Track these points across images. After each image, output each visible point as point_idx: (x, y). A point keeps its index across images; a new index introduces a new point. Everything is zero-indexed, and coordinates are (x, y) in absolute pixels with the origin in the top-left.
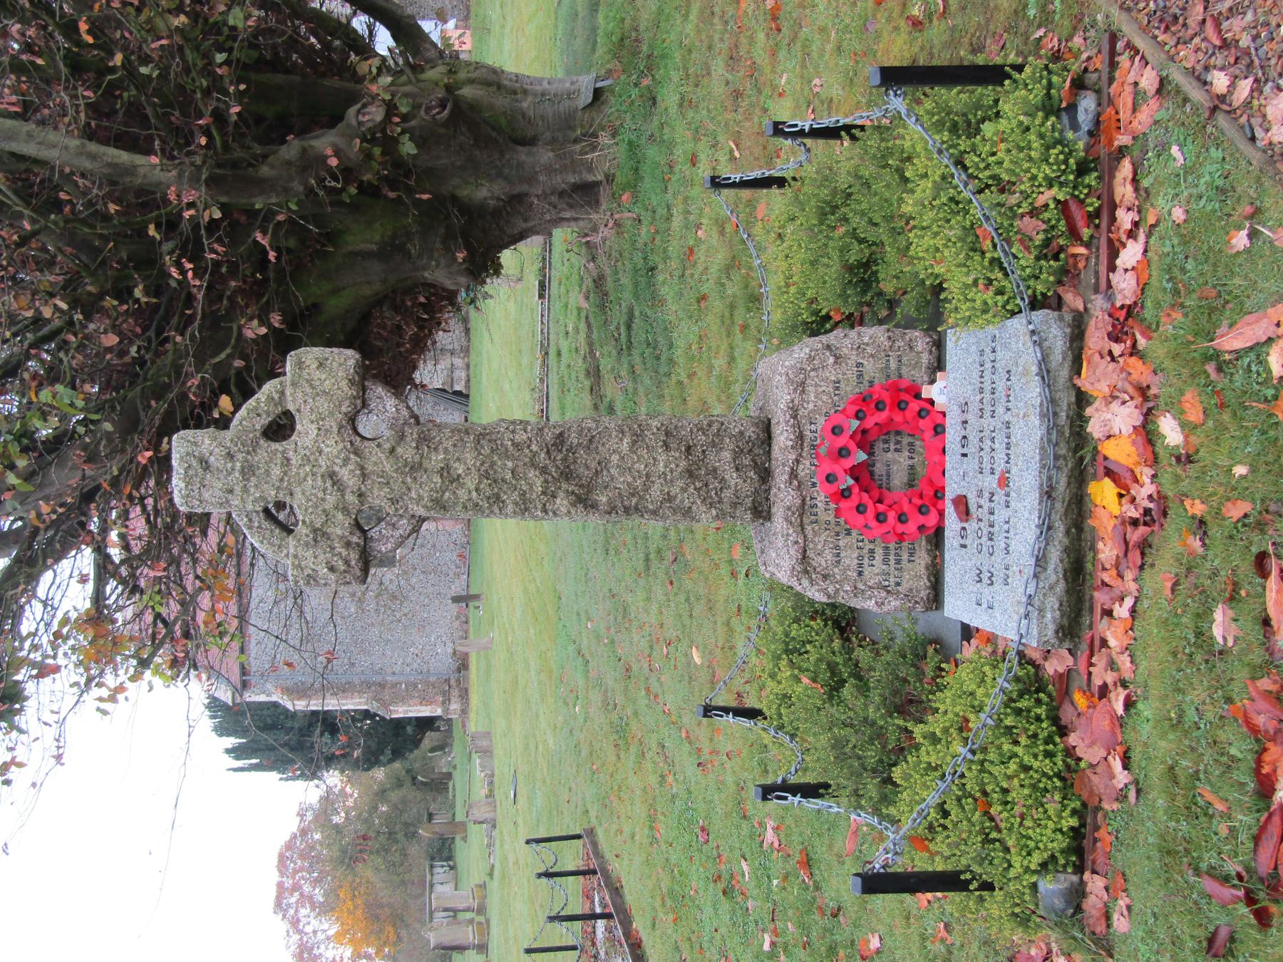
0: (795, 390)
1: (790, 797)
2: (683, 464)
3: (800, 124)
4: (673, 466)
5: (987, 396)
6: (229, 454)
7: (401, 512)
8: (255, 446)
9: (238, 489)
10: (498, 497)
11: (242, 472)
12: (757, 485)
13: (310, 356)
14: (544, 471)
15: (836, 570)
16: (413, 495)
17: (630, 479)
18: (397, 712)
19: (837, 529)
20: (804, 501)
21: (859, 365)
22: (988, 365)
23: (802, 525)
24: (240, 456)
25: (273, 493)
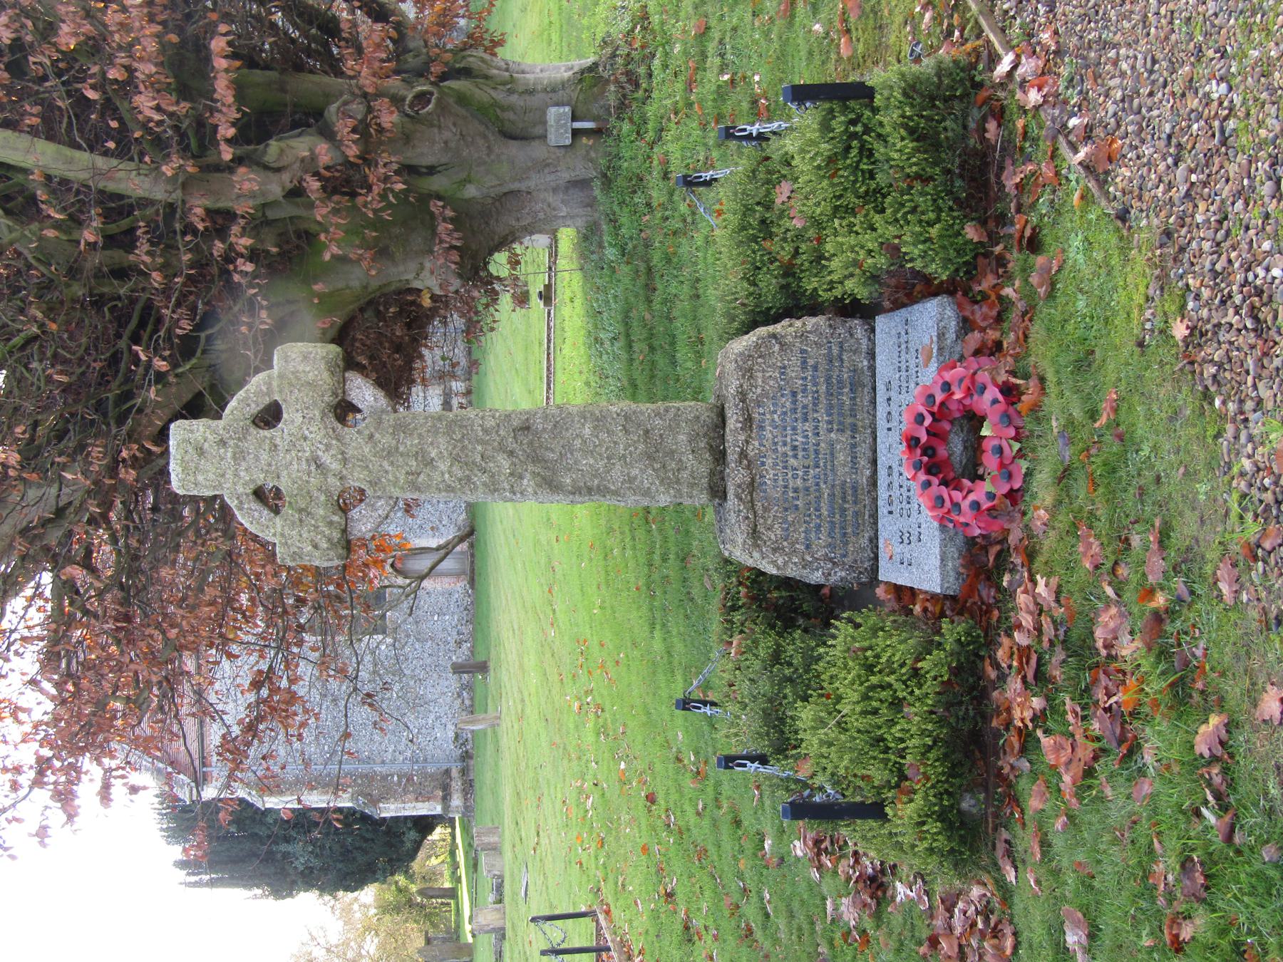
0: (743, 376)
1: (749, 764)
2: (641, 447)
3: (748, 128)
4: (632, 449)
5: (904, 373)
6: (221, 440)
7: (379, 493)
8: (246, 431)
9: (229, 475)
10: (468, 479)
11: (234, 458)
12: (712, 466)
13: (296, 350)
14: (511, 453)
15: (785, 544)
16: (390, 477)
17: (592, 461)
18: (387, 810)
19: (786, 505)
20: (753, 480)
21: (803, 351)
22: (903, 346)
23: (752, 501)
24: (231, 443)
25: (262, 476)
